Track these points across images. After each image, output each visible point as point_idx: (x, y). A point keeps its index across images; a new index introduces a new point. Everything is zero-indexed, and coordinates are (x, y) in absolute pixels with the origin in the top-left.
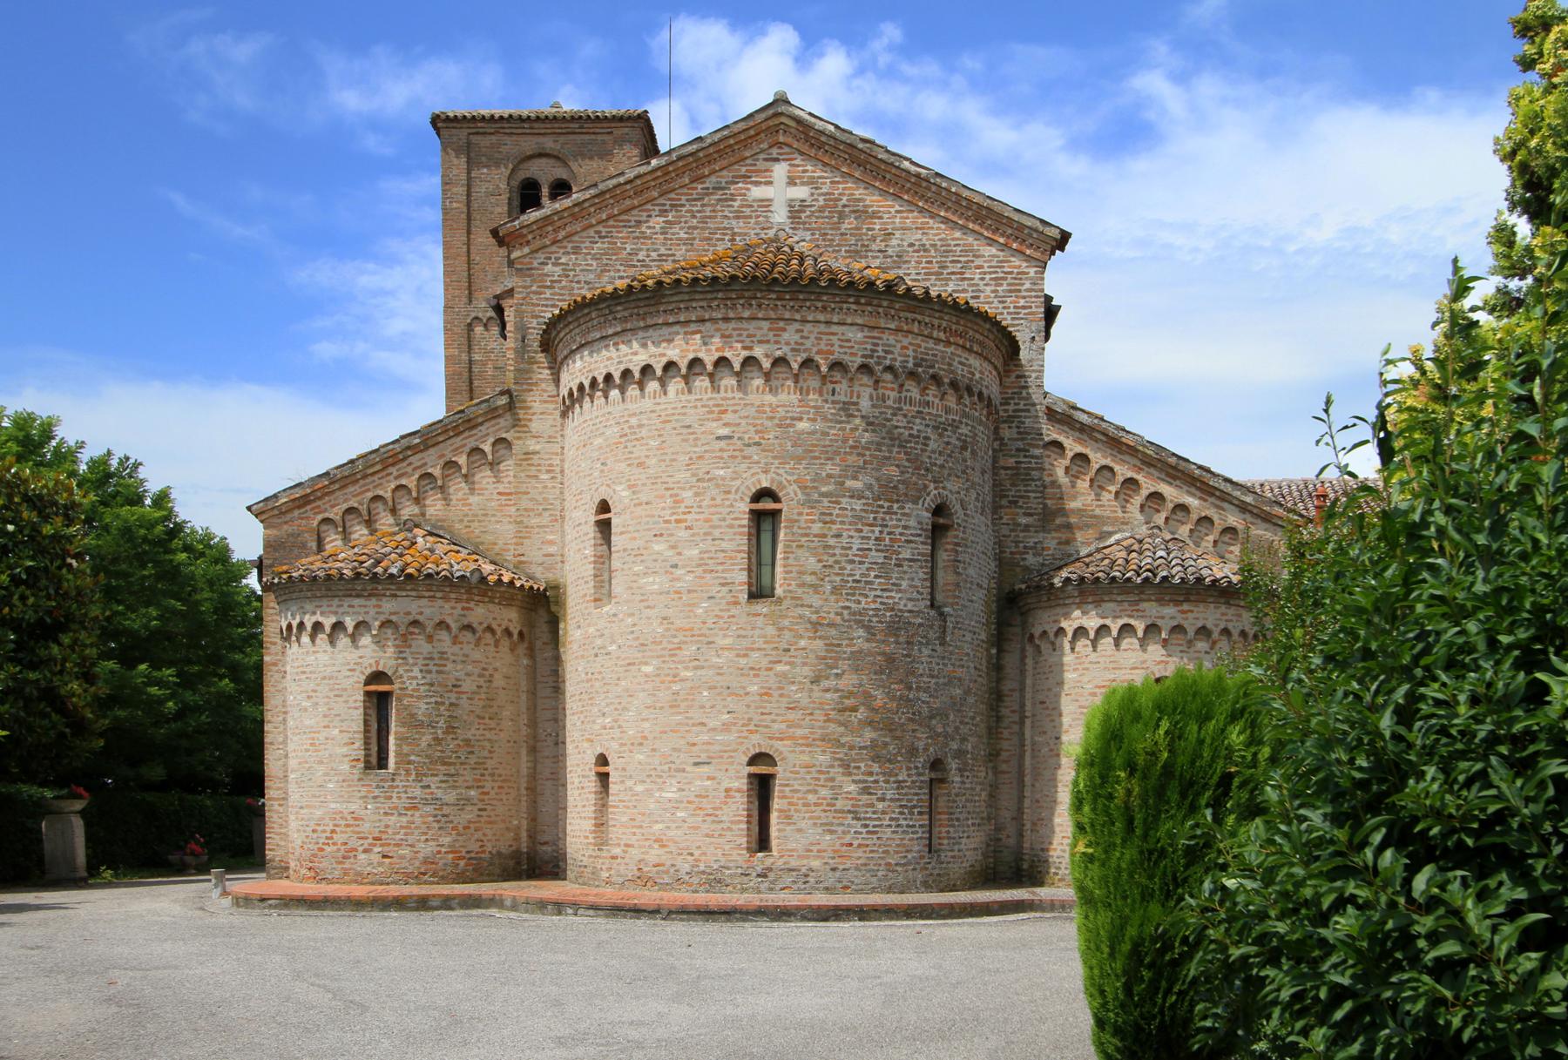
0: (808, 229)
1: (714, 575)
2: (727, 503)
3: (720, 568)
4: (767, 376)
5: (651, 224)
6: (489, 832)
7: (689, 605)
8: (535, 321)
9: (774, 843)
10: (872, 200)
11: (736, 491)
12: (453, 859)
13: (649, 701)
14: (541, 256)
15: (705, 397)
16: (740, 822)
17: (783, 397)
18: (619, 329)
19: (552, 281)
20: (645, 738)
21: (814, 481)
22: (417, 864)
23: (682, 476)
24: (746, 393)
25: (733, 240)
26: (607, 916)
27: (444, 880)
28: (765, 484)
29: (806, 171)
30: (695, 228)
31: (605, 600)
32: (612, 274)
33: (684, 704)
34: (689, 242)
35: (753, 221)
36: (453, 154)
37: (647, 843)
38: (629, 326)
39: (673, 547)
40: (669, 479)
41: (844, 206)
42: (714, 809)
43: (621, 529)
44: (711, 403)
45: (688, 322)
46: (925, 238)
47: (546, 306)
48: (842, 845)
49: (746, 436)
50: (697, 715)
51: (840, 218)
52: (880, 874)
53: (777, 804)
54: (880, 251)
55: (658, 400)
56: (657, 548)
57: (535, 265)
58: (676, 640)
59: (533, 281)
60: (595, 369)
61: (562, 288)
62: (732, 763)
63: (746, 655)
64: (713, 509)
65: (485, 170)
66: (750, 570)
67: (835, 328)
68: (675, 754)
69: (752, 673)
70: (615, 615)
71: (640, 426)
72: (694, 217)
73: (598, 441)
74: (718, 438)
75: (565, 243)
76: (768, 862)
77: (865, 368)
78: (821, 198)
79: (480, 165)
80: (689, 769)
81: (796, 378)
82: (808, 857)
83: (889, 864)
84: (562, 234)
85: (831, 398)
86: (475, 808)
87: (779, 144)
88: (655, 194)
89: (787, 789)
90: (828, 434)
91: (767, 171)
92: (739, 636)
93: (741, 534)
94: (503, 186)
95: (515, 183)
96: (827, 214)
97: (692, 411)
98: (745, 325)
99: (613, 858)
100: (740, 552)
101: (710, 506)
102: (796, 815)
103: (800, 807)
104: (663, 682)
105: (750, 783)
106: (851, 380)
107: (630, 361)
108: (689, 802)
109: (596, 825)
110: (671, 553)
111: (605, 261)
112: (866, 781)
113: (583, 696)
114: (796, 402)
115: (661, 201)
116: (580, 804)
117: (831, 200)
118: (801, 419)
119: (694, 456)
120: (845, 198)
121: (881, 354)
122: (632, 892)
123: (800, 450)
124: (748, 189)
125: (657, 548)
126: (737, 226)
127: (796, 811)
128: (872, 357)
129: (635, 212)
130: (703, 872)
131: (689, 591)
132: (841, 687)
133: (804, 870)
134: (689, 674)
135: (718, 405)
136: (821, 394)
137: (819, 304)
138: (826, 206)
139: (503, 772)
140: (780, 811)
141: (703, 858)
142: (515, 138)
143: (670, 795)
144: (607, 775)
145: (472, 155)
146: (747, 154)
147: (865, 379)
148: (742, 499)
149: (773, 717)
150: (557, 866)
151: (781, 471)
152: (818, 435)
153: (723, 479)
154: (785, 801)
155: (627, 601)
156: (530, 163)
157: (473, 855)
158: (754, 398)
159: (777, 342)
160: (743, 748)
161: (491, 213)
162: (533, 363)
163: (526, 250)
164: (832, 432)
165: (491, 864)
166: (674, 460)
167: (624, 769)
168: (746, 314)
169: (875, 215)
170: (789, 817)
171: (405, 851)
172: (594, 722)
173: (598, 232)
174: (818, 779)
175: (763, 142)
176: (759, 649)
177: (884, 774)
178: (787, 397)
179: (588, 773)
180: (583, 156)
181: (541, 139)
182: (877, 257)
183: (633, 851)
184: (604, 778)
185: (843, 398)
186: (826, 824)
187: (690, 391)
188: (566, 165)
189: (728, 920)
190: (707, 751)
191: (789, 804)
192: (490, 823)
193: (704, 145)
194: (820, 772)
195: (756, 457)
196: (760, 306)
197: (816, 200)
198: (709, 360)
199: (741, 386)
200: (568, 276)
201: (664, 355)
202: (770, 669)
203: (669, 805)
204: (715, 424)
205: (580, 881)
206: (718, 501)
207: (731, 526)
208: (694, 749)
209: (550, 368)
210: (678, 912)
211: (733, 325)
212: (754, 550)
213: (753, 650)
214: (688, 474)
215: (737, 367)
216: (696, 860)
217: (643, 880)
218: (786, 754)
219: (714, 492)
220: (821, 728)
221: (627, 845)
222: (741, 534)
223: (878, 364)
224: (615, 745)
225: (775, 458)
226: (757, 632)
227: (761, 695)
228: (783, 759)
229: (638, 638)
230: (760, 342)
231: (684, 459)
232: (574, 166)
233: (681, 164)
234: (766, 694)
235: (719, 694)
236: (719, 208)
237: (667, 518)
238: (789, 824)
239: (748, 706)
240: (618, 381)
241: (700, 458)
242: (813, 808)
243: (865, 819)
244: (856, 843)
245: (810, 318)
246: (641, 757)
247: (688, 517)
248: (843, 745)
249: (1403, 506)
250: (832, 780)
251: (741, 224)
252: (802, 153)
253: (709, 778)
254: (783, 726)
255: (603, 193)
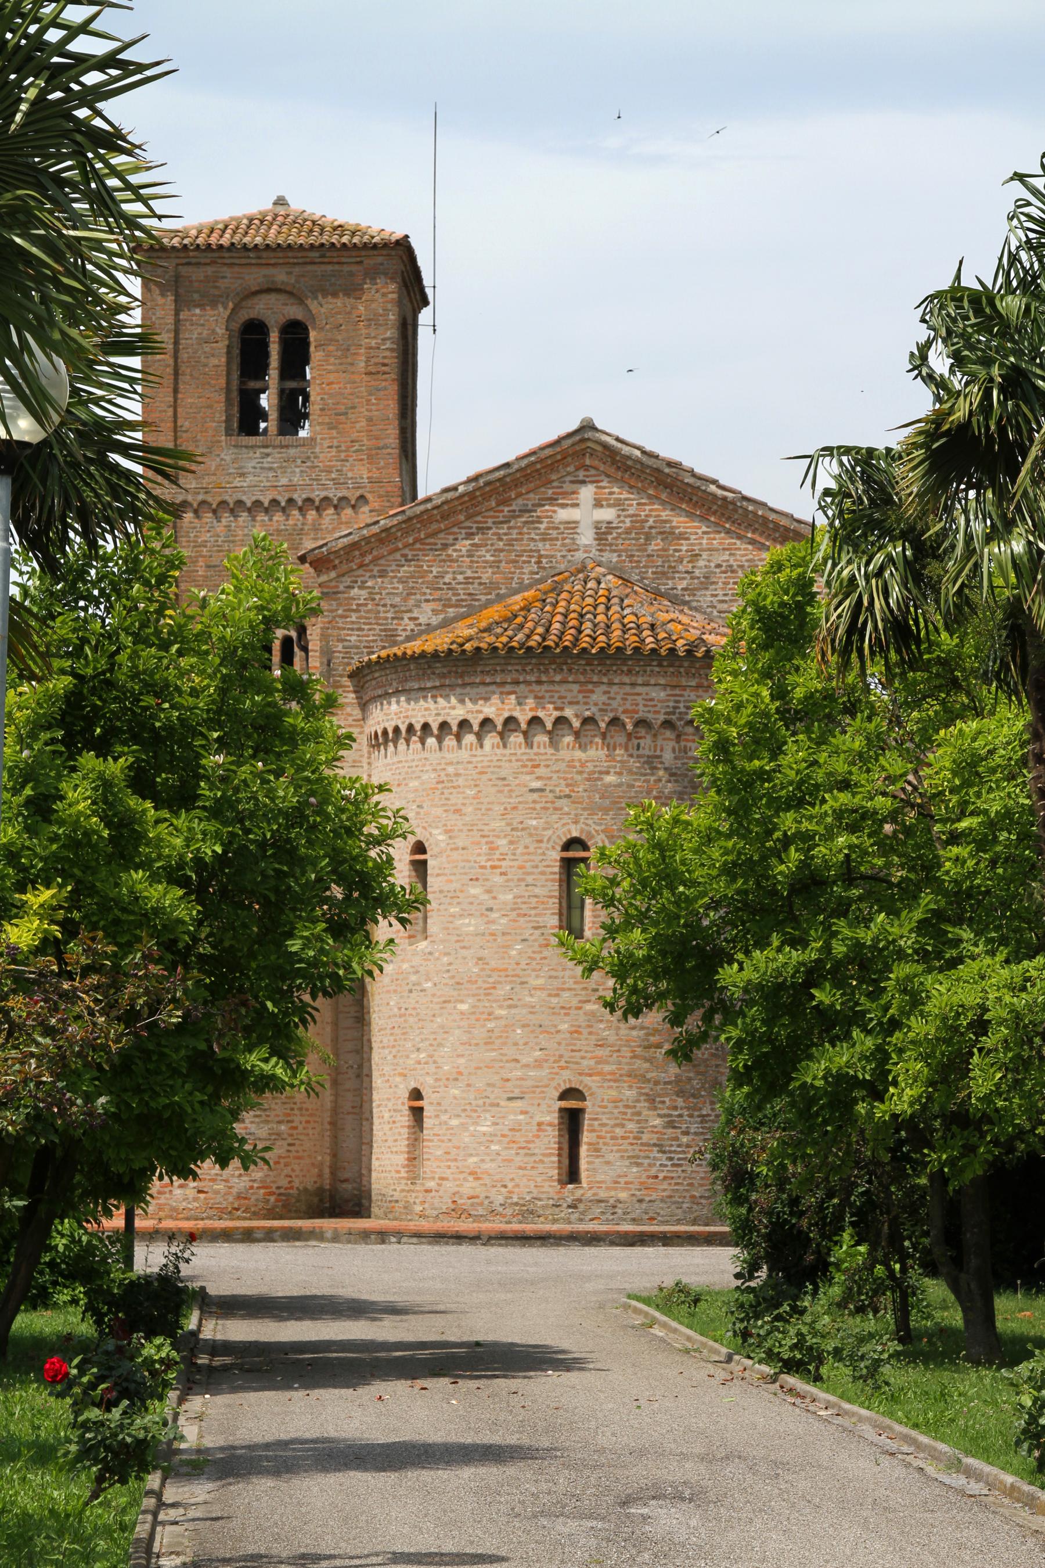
0: (615, 551)
1: (527, 918)
2: (540, 851)
3: (533, 912)
4: (577, 734)
5: (457, 547)
6: (296, 1167)
7: (503, 947)
8: (340, 645)
9: (584, 1175)
10: (679, 522)
11: (549, 840)
12: (265, 1194)
13: (465, 1038)
14: (347, 580)
15: (519, 752)
16: (551, 1154)
17: (592, 753)
18: (438, 684)
19: (358, 605)
20: (460, 1073)
21: (620, 830)
22: (231, 1199)
23: (498, 824)
24: (557, 749)
25: (539, 562)
26: (430, 1243)
27: (256, 1216)
28: (575, 834)
29: (611, 493)
30: (502, 551)
31: (419, 937)
32: (418, 597)
33: (498, 1042)
34: (496, 565)
35: (559, 543)
36: (156, 291)
37: (462, 1176)
38: (447, 682)
39: (488, 892)
40: (486, 828)
41: (651, 527)
42: (528, 1142)
43: (437, 871)
44: (525, 757)
45: (503, 684)
46: (732, 559)
47: (352, 629)
48: (648, 1177)
49: (558, 789)
50: (511, 1052)
51: (647, 539)
52: (685, 1206)
53: (586, 1137)
54: (687, 572)
55: (474, 752)
56: (473, 891)
57: (341, 588)
58: (491, 980)
59: (339, 605)
60: (415, 716)
61: (368, 612)
62: (544, 1098)
63: (557, 995)
64: (526, 857)
65: (198, 311)
66: (560, 914)
67: (639, 689)
68: (490, 1089)
69: (563, 1011)
70: (430, 953)
71: (457, 775)
72: (500, 539)
73: (414, 784)
74: (532, 791)
75: (371, 567)
76: (578, 1193)
77: (668, 724)
78: (628, 520)
79: (191, 304)
80: (502, 1103)
81: (604, 736)
82: (616, 1189)
83: (693, 1197)
84: (368, 558)
85: (635, 753)
86: (285, 1143)
87: (587, 468)
88: (462, 517)
89: (596, 1123)
90: (633, 786)
91: (574, 493)
92: (550, 977)
93: (553, 880)
94: (221, 331)
95: (236, 326)
96: (633, 535)
97: (507, 765)
98: (557, 687)
99: (427, 1191)
100: (551, 897)
101: (523, 854)
102: (604, 1148)
103: (608, 1140)
104: (478, 1020)
105: (561, 1117)
106: (655, 736)
107: (448, 714)
108: (503, 1136)
109: (409, 1159)
110: (486, 897)
111: (411, 585)
112: (670, 1115)
113: (396, 1031)
114: (604, 758)
115: (467, 524)
116: (391, 1139)
117: (636, 522)
118: (608, 773)
119: (509, 806)
120: (651, 520)
121: (683, 710)
122: (445, 1224)
123: (607, 801)
124: (554, 512)
125: (473, 891)
126: (544, 548)
127: (605, 1144)
128: (674, 713)
129: (441, 535)
130: (516, 1204)
131: (504, 934)
132: (646, 1025)
133: (612, 1201)
134: (503, 1012)
135: (531, 760)
136: (626, 750)
137: (625, 668)
138: (633, 528)
139: (310, 1107)
140: (589, 1144)
141: (516, 1190)
142: (236, 269)
143: (484, 1129)
144: (421, 1109)
145: (181, 291)
146: (554, 477)
147: (668, 734)
148: (553, 848)
149: (582, 1053)
150: (359, 1205)
151: (590, 822)
152: (624, 788)
153: (536, 828)
154: (594, 1134)
155: (442, 941)
156: (256, 300)
157: (282, 1191)
158: (564, 754)
159: (586, 703)
160: (554, 1084)
161: (205, 365)
162: (338, 687)
163: (333, 574)
164: (637, 784)
165: (298, 1201)
166: (489, 809)
167: (439, 1104)
168: (558, 678)
169: (681, 536)
170: (598, 1150)
171: (220, 1187)
172: (408, 1057)
173: (404, 556)
174: (625, 1114)
175: (567, 465)
176: (570, 989)
177: (688, 1108)
178: (596, 753)
179: (400, 1107)
180: (325, 293)
181: (271, 271)
182: (684, 578)
183: (447, 1184)
184: (417, 1113)
185: (647, 752)
186: (633, 1157)
187: (505, 746)
188: (301, 301)
189: (543, 1245)
190: (521, 1086)
191: (599, 1137)
192: (298, 1158)
193: (511, 471)
194: (627, 1107)
195: (566, 809)
196: (570, 670)
197: (623, 522)
198: (523, 718)
199: (554, 743)
200: (373, 599)
201: (481, 712)
202: (580, 1008)
203: (484, 1139)
204: (528, 777)
205: (390, 1216)
206: (531, 850)
207: (543, 873)
208: (509, 1084)
209: (355, 692)
210: (497, 1238)
211: (545, 687)
212: (565, 895)
213: (563, 990)
214: (503, 823)
215: (549, 726)
216: (510, 1192)
217: (457, 1211)
218: (594, 1089)
219: (528, 841)
220: (627, 1064)
221: (442, 1179)
222: (553, 880)
223: (680, 719)
224: (430, 1080)
225: (584, 809)
226: (568, 973)
227: (571, 1033)
228: (591, 1094)
229: (453, 977)
230: (570, 703)
231: (498, 809)
232: (313, 305)
233: (488, 489)
234: (576, 1032)
235: (533, 1032)
236: (525, 530)
237: (483, 863)
238: (598, 1157)
239: (559, 1044)
240: (435, 731)
241: (515, 808)
242: (620, 1141)
243: (670, 1152)
244: (661, 1175)
245: (616, 681)
246: (456, 1092)
247: (503, 863)
248: (649, 1081)
249: (827, 1002)
250: (639, 1114)
251: (548, 547)
252: (608, 476)
253: (522, 1113)
254: (592, 1062)
255: (410, 519)
